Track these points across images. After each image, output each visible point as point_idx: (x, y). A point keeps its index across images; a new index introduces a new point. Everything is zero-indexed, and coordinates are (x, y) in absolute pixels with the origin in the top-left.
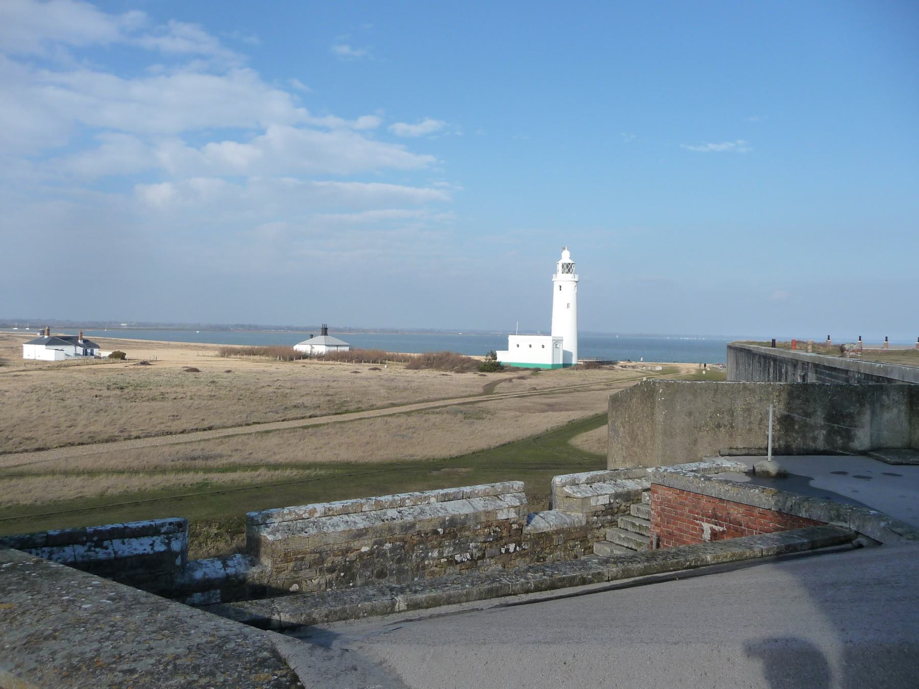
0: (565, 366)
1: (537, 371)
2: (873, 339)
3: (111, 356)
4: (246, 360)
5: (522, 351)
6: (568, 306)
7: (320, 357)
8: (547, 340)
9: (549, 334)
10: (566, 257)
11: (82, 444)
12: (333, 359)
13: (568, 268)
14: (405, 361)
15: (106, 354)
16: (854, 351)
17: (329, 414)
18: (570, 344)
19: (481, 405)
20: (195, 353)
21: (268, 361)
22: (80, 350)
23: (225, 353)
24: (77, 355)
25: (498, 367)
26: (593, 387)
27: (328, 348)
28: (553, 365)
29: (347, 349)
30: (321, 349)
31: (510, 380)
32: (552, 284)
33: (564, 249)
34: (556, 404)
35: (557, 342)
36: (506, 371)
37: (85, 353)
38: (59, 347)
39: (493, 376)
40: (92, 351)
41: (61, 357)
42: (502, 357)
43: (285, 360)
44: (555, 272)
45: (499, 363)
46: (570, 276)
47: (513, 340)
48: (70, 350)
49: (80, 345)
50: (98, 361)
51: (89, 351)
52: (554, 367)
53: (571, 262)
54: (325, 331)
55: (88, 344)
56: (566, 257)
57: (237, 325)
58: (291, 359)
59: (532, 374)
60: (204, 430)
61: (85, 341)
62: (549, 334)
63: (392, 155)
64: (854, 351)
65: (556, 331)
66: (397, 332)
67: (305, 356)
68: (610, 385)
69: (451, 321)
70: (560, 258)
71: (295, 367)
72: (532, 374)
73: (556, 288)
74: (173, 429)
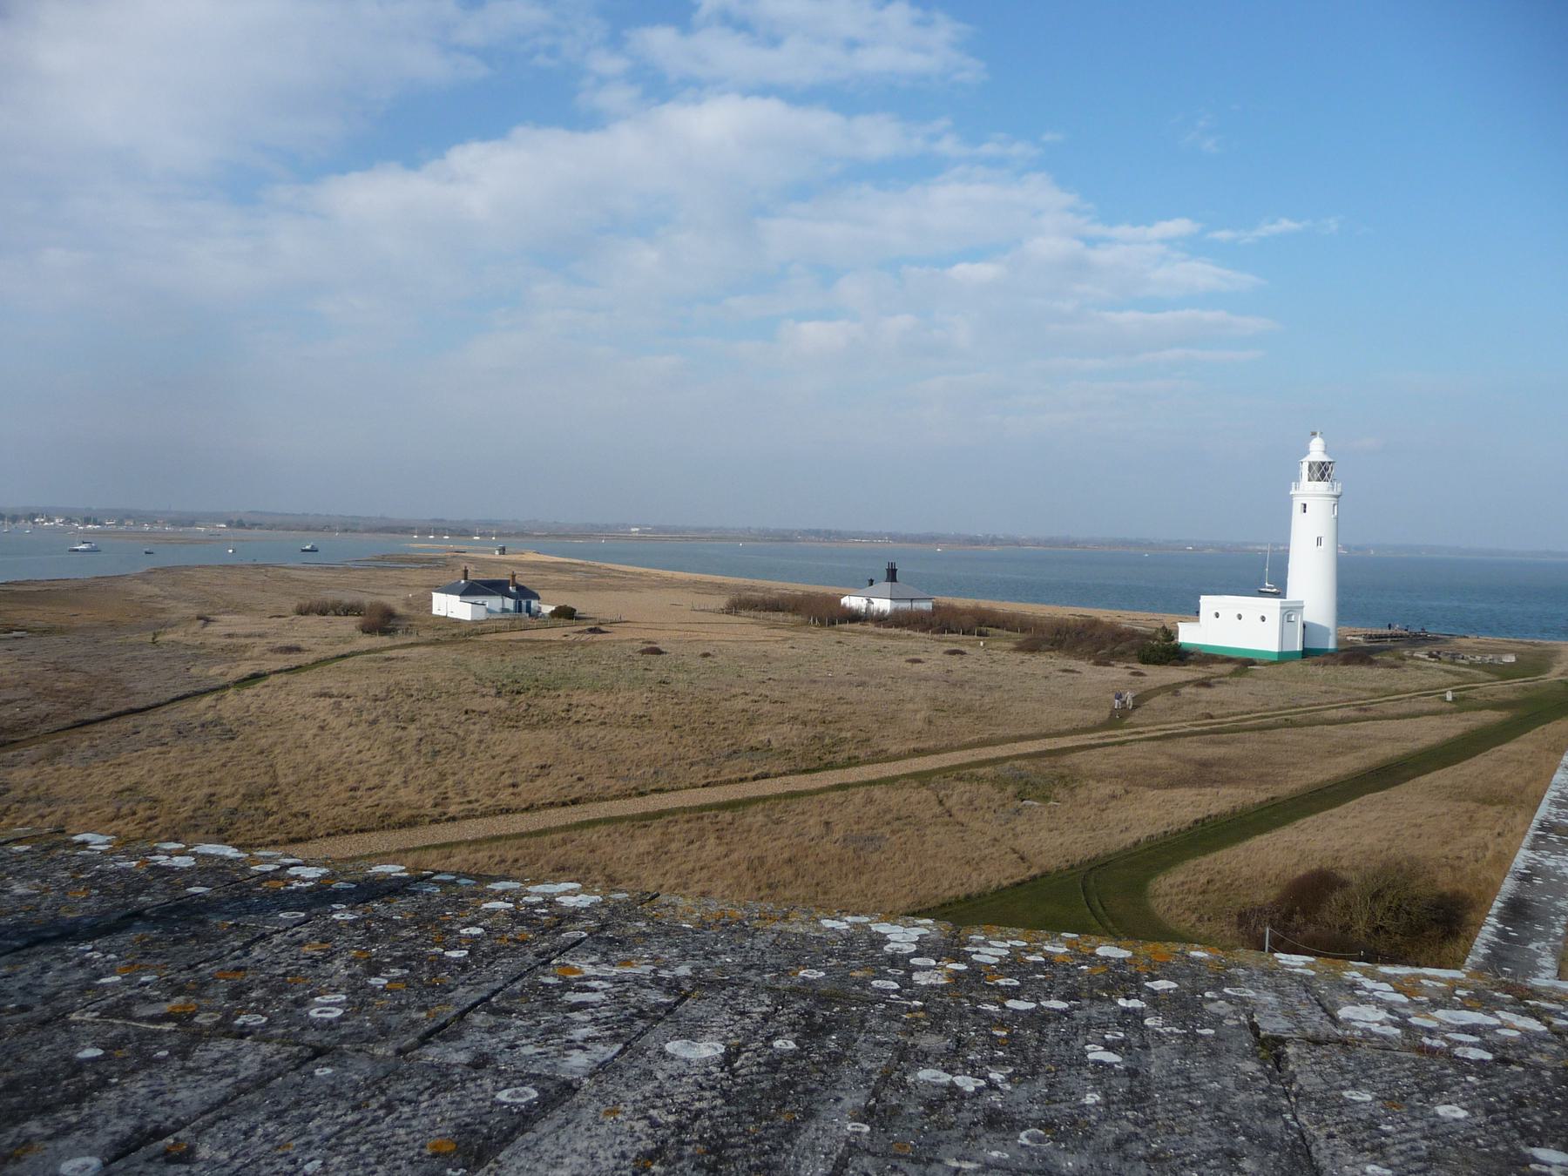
0: (1306, 653)
1: (1243, 664)
3: (553, 614)
5: (1227, 624)
7: (881, 619)
8: (1272, 606)
9: (1280, 594)
10: (1316, 451)
11: (362, 831)
13: (1322, 471)
14: (1022, 631)
15: (547, 609)
17: (792, 772)
19: (1076, 758)
21: (796, 627)
22: (510, 603)
24: (504, 610)
25: (1178, 655)
27: (896, 604)
28: (1280, 654)
30: (883, 605)
31: (1174, 689)
33: (1314, 434)
34: (1222, 761)
35: (1288, 614)
36: (1190, 662)
37: (519, 609)
38: (480, 599)
39: (1159, 675)
40: (529, 604)
41: (481, 614)
42: (1189, 635)
43: (822, 624)
44: (1296, 478)
45: (1178, 646)
46: (1322, 486)
47: (1207, 603)
48: (495, 602)
49: (510, 595)
50: (536, 623)
51: (524, 603)
52: (1284, 658)
53: (1326, 459)
55: (524, 593)
57: (809, 532)
59: (1234, 674)
60: (564, 804)
61: (519, 588)
62: (1280, 594)
63: (1202, 274)
65: (1294, 592)
66: (1074, 544)
67: (854, 617)
70: (1307, 452)
71: (822, 639)
72: (1234, 674)
73: (1297, 507)
74: (537, 798)
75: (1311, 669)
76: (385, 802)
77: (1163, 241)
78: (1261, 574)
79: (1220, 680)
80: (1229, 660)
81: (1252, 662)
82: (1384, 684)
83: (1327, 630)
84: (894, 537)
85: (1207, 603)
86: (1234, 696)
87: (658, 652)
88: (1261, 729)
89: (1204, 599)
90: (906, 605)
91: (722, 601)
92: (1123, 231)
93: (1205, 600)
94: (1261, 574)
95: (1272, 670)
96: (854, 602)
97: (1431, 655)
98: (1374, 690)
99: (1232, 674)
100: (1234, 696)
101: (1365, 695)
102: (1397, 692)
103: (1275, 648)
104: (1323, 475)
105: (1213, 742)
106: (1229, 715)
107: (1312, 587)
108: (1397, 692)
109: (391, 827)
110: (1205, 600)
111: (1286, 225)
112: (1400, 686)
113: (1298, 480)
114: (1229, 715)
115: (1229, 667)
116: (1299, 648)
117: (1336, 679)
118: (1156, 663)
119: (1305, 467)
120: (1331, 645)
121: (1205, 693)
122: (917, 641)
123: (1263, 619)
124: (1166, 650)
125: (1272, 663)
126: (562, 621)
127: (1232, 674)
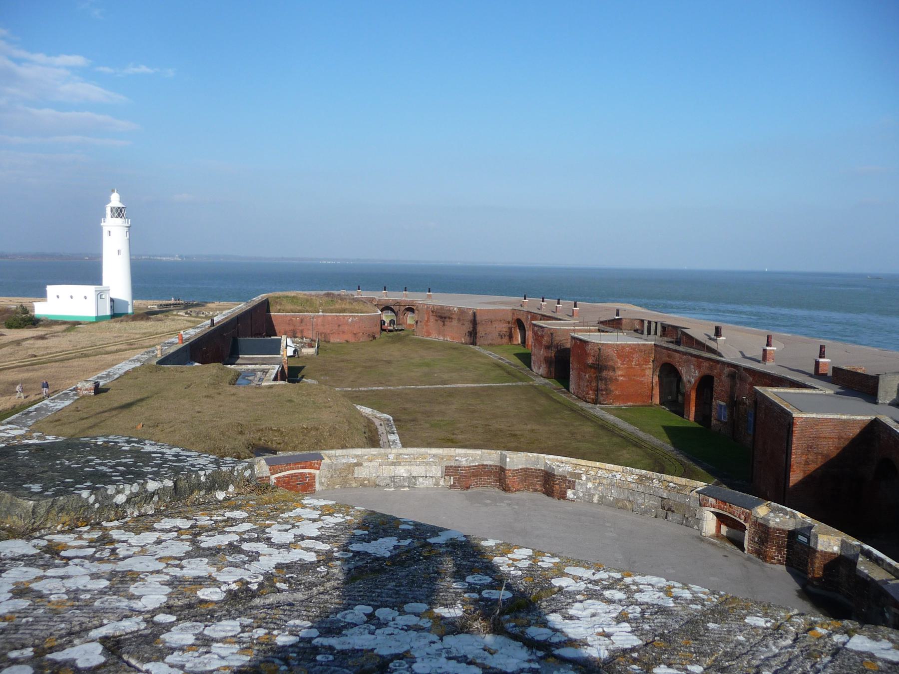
1: (73, 325)
6: (119, 252)
8: (90, 290)
10: (115, 200)
13: (119, 212)
16: (86, 390)
26: (108, 349)
28: (97, 317)
32: (100, 230)
33: (113, 191)
36: (40, 326)
42: (40, 309)
46: (119, 221)
47: (51, 290)
52: (99, 319)
53: (121, 205)
56: (115, 200)
63: (94, 92)
64: (86, 390)
68: (131, 344)
70: (109, 201)
75: (118, 325)
76: (196, 654)
77: (68, 68)
78: (88, 272)
79: (54, 335)
80: (64, 323)
81: (79, 323)
82: (151, 330)
83: (127, 302)
85: (51, 290)
86: (61, 343)
88: (62, 360)
92: (40, 57)
93: (50, 288)
94: (88, 272)
95: (89, 327)
97: (186, 313)
98: (144, 333)
99: (64, 331)
100: (61, 343)
101: (137, 336)
102: (157, 334)
104: (119, 215)
105: (28, 370)
106: (48, 354)
107: (117, 280)
108: (157, 334)
110: (50, 288)
111: (143, 69)
112: (159, 331)
113: (105, 217)
114: (48, 354)
115: (64, 327)
116: (108, 313)
117: (125, 329)
118: (16, 328)
120: (130, 311)
121: (40, 343)
123: (86, 298)
124: (23, 320)
125: (91, 323)
127: (64, 331)
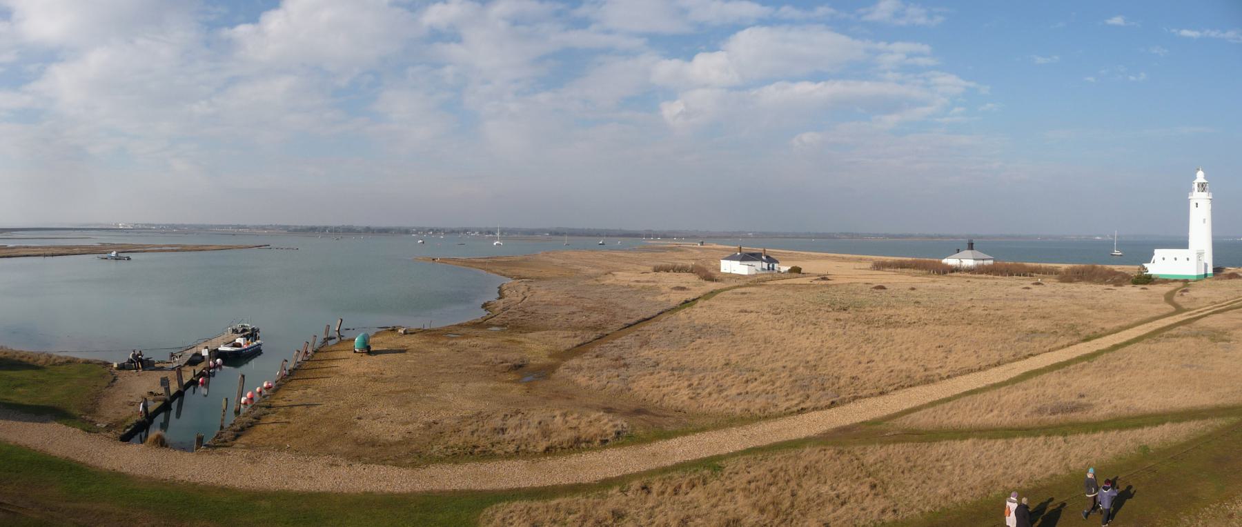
2: (16, 348)
3: (790, 271)
4: (902, 273)
5: (1163, 263)
7: (970, 270)
12: (982, 273)
13: (1202, 187)
18: (1208, 258)
20: (852, 265)
21: (923, 275)
22: (765, 265)
23: (879, 266)
25: (1149, 280)
29: (991, 262)
30: (969, 263)
42: (1153, 269)
43: (939, 273)
44: (1191, 190)
46: (1205, 194)
47: (1159, 253)
48: (758, 265)
52: (1199, 279)
54: (971, 246)
55: (770, 260)
56: (1200, 177)
58: (945, 273)
69: (1104, 225)
71: (942, 282)
84: (887, 236)
85: (1159, 253)
87: (882, 288)
89: (1156, 251)
90: (981, 262)
91: (869, 265)
96: (951, 261)
103: (1195, 274)
109: (1020, 359)
119: (1196, 186)
122: (990, 280)
126: (795, 275)
